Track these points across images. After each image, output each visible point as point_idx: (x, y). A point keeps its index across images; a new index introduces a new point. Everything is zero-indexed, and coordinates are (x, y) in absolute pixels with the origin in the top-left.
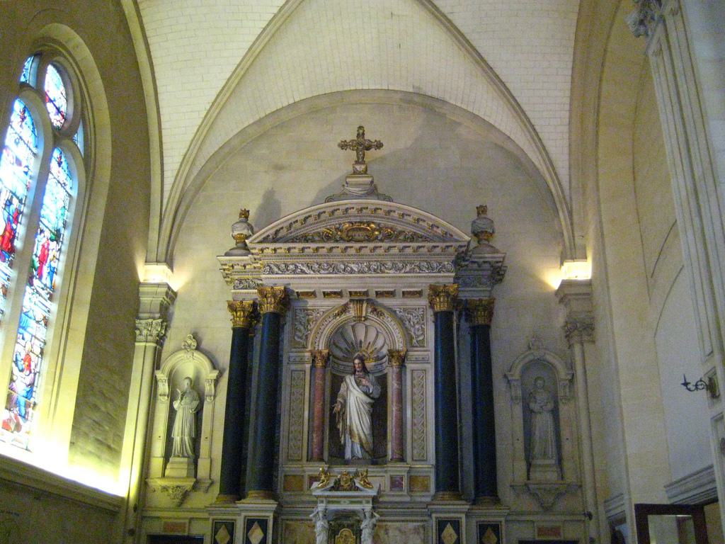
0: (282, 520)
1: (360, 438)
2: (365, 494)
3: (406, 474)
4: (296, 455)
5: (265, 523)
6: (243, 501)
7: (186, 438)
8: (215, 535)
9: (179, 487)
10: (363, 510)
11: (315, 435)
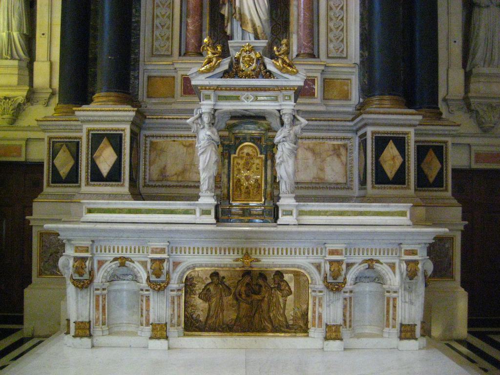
0: (146, 137)
1: (254, 26)
2: (285, 84)
3: (318, 75)
4: (164, 49)
5: (118, 140)
6: (85, 107)
7: (15, 34)
8: (53, 158)
9: (9, 99)
10: (279, 111)
11: (189, 21)
